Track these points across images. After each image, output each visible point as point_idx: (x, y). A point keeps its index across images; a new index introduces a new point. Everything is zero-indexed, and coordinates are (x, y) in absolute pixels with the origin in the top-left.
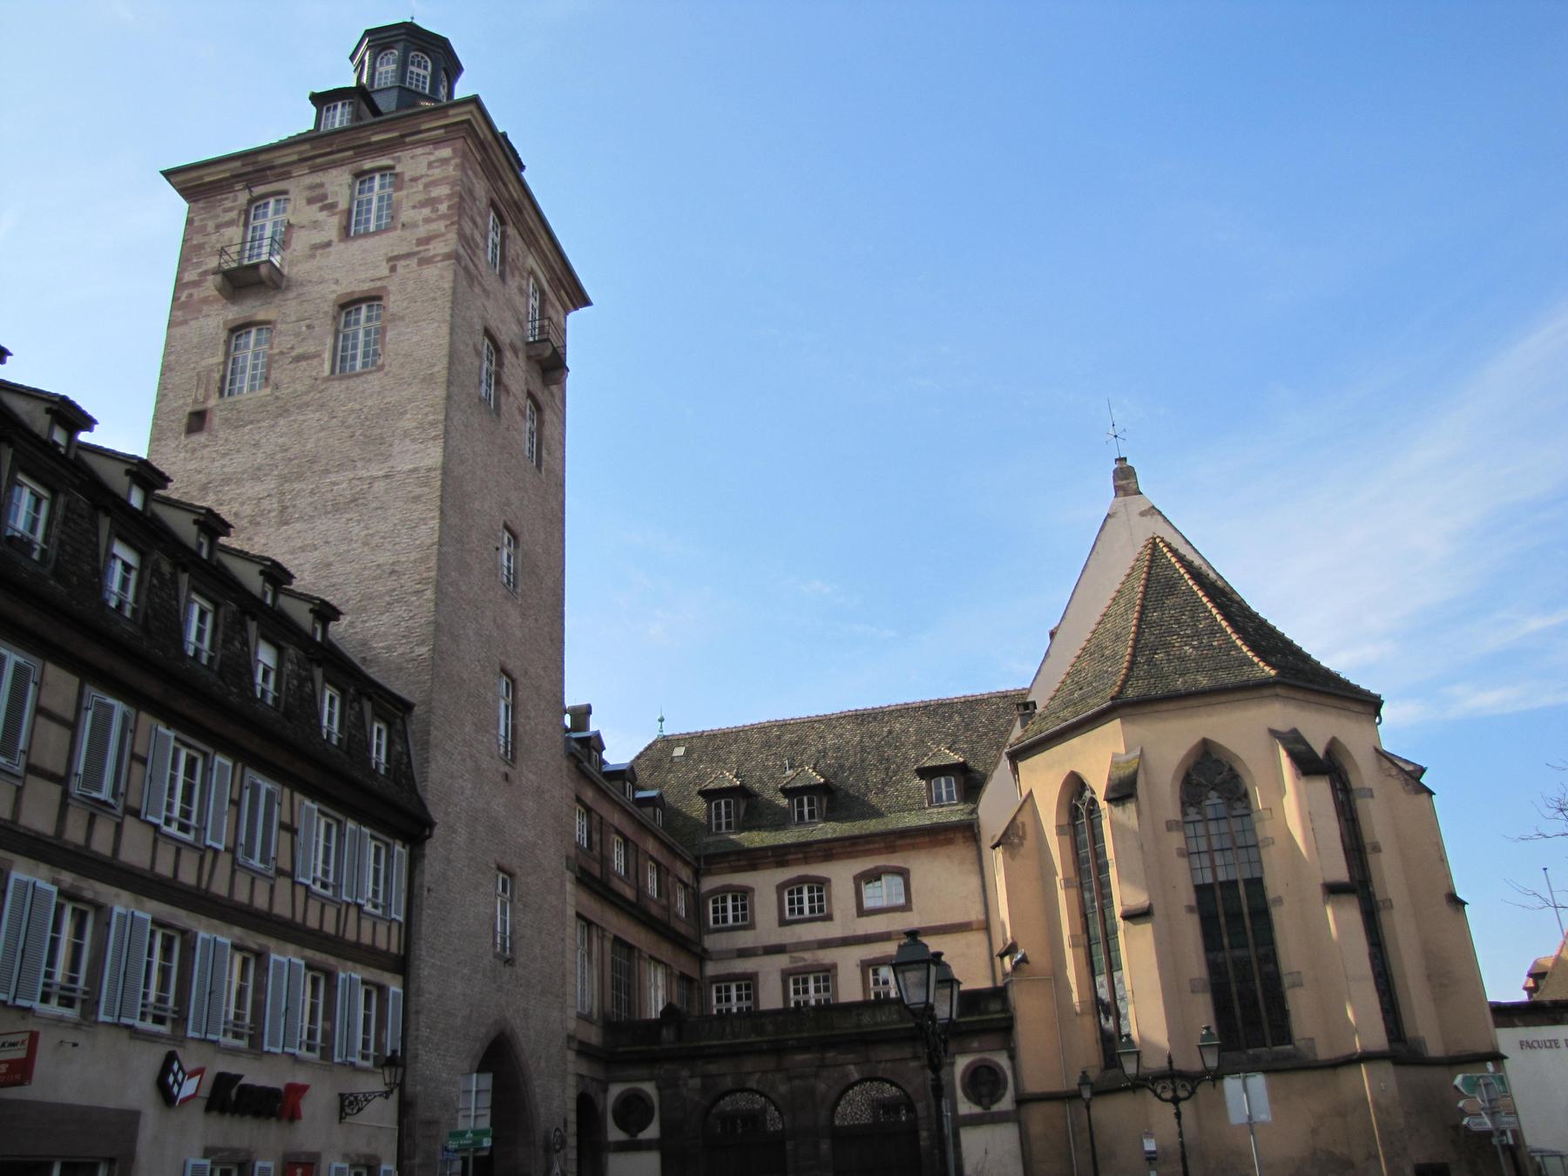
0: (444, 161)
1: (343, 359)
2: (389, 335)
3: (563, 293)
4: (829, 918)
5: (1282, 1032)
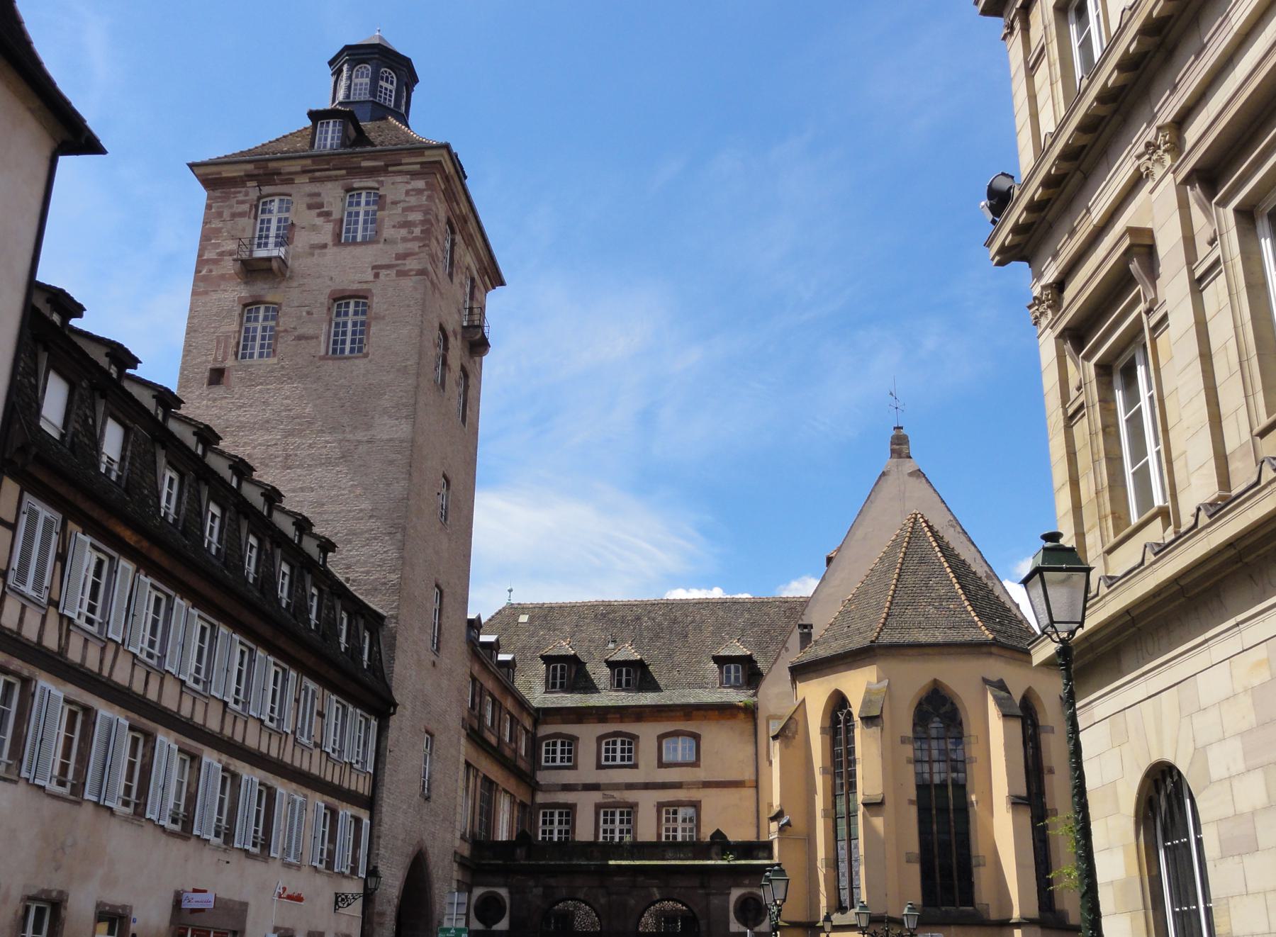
0: (419, 192)
1: (335, 342)
2: (373, 329)
3: (486, 278)
4: (635, 766)
5: (967, 894)
